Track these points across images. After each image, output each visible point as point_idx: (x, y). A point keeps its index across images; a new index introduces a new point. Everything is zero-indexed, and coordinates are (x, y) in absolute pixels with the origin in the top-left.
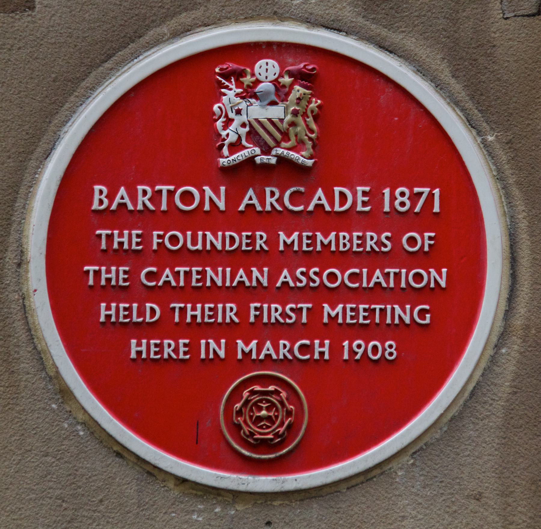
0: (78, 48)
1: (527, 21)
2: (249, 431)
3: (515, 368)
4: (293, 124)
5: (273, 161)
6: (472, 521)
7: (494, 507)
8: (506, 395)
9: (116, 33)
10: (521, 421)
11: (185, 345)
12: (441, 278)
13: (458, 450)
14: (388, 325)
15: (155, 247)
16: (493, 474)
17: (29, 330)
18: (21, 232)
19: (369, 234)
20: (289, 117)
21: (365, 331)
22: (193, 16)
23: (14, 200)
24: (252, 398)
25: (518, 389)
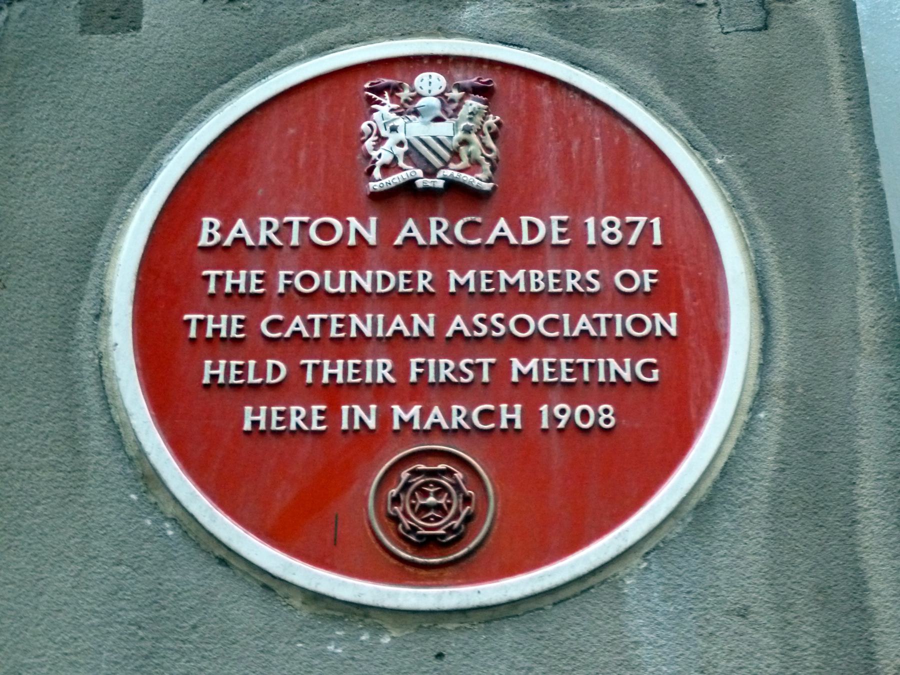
0: (191, 68)
1: (751, 35)
2: (410, 525)
3: (779, 437)
4: (465, 142)
5: (440, 184)
6: (737, 646)
7: (768, 625)
8: (770, 473)
9: (240, 52)
10: (795, 508)
11: (320, 413)
12: (669, 323)
13: (709, 548)
14: (602, 384)
15: (281, 289)
16: (762, 581)
17: (105, 397)
18: (102, 277)
19: (569, 272)
20: (460, 135)
21: (571, 391)
22: (337, 33)
23: (97, 239)
24: (414, 480)
25: (787, 464)
